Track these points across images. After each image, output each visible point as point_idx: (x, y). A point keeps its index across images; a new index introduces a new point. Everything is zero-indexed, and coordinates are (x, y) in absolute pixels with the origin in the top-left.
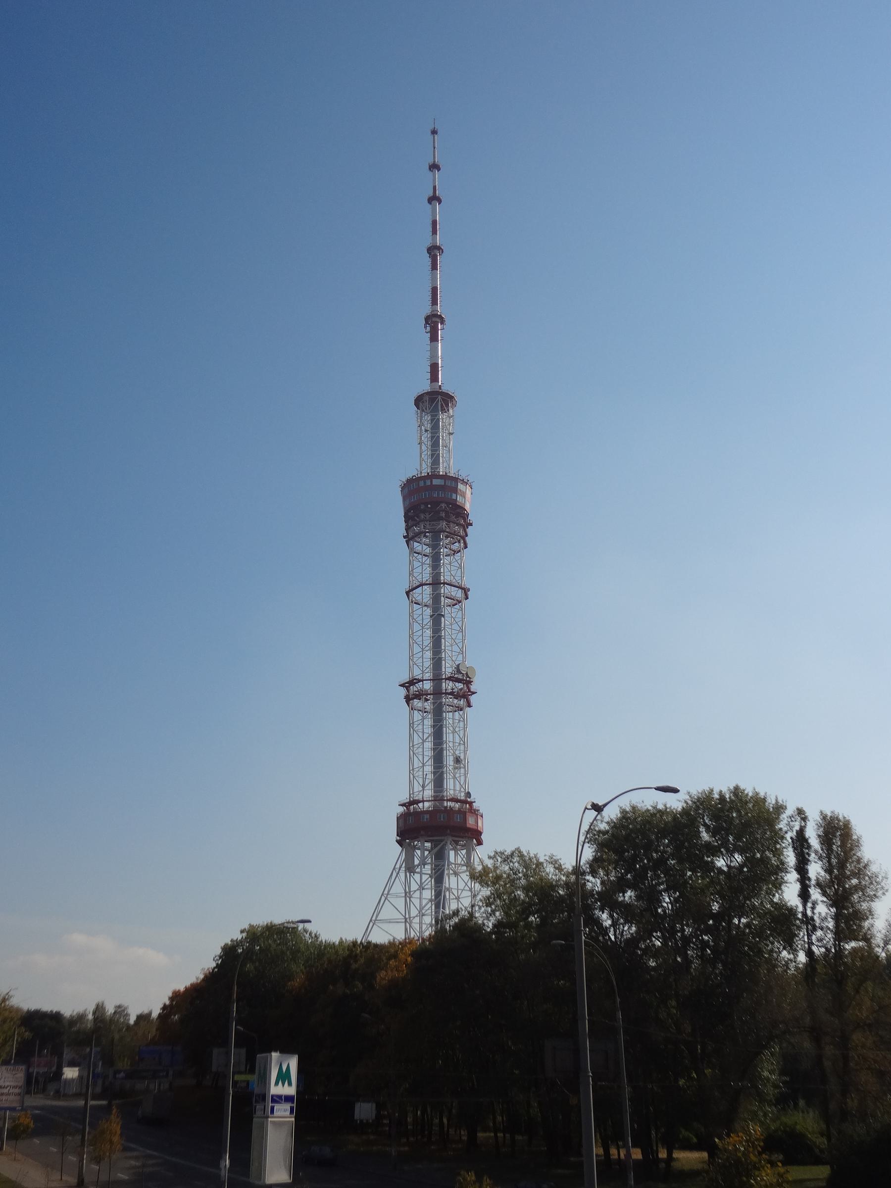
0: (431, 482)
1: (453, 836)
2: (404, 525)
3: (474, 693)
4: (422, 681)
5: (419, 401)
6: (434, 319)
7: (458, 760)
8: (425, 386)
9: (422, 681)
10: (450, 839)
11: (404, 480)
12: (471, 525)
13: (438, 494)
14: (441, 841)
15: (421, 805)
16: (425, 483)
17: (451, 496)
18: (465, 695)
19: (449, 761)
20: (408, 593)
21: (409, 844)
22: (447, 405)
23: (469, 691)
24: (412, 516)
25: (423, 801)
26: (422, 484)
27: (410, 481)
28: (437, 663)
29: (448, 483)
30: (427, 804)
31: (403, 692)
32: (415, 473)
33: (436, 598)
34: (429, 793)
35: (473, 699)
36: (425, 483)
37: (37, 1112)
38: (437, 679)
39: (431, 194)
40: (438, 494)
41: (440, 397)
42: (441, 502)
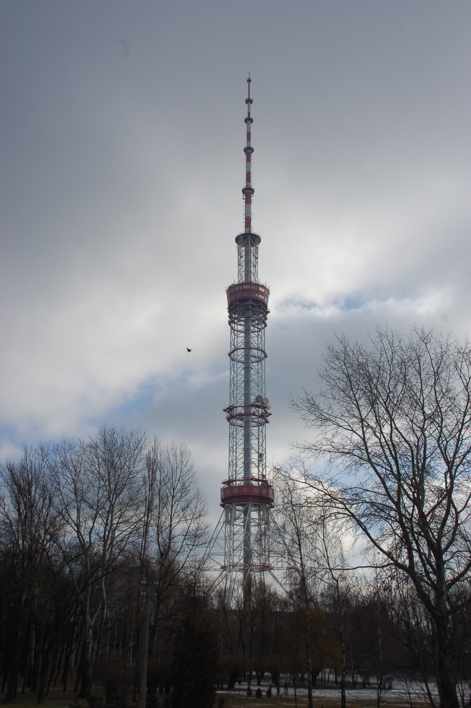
0: (242, 287)
1: (252, 501)
2: (228, 314)
3: (270, 414)
4: (236, 407)
5: (238, 239)
6: (248, 191)
7: (260, 456)
8: (242, 230)
9: (236, 407)
10: (251, 503)
11: (228, 287)
12: (269, 312)
13: (247, 294)
14: (246, 504)
15: (234, 483)
16: (239, 288)
17: (255, 295)
18: (264, 417)
19: (254, 457)
20: (230, 355)
21: (228, 507)
22: (254, 241)
23: (267, 413)
24: (233, 308)
25: (236, 481)
26: (237, 289)
27: (230, 288)
28: (247, 395)
29: (253, 287)
30: (238, 483)
31: (226, 414)
32: (233, 283)
33: (247, 356)
34: (241, 476)
35: (269, 418)
36: (239, 288)
37: (459, 698)
38: (247, 406)
39: (246, 116)
40: (247, 294)
41: (249, 237)
42: (249, 299)
